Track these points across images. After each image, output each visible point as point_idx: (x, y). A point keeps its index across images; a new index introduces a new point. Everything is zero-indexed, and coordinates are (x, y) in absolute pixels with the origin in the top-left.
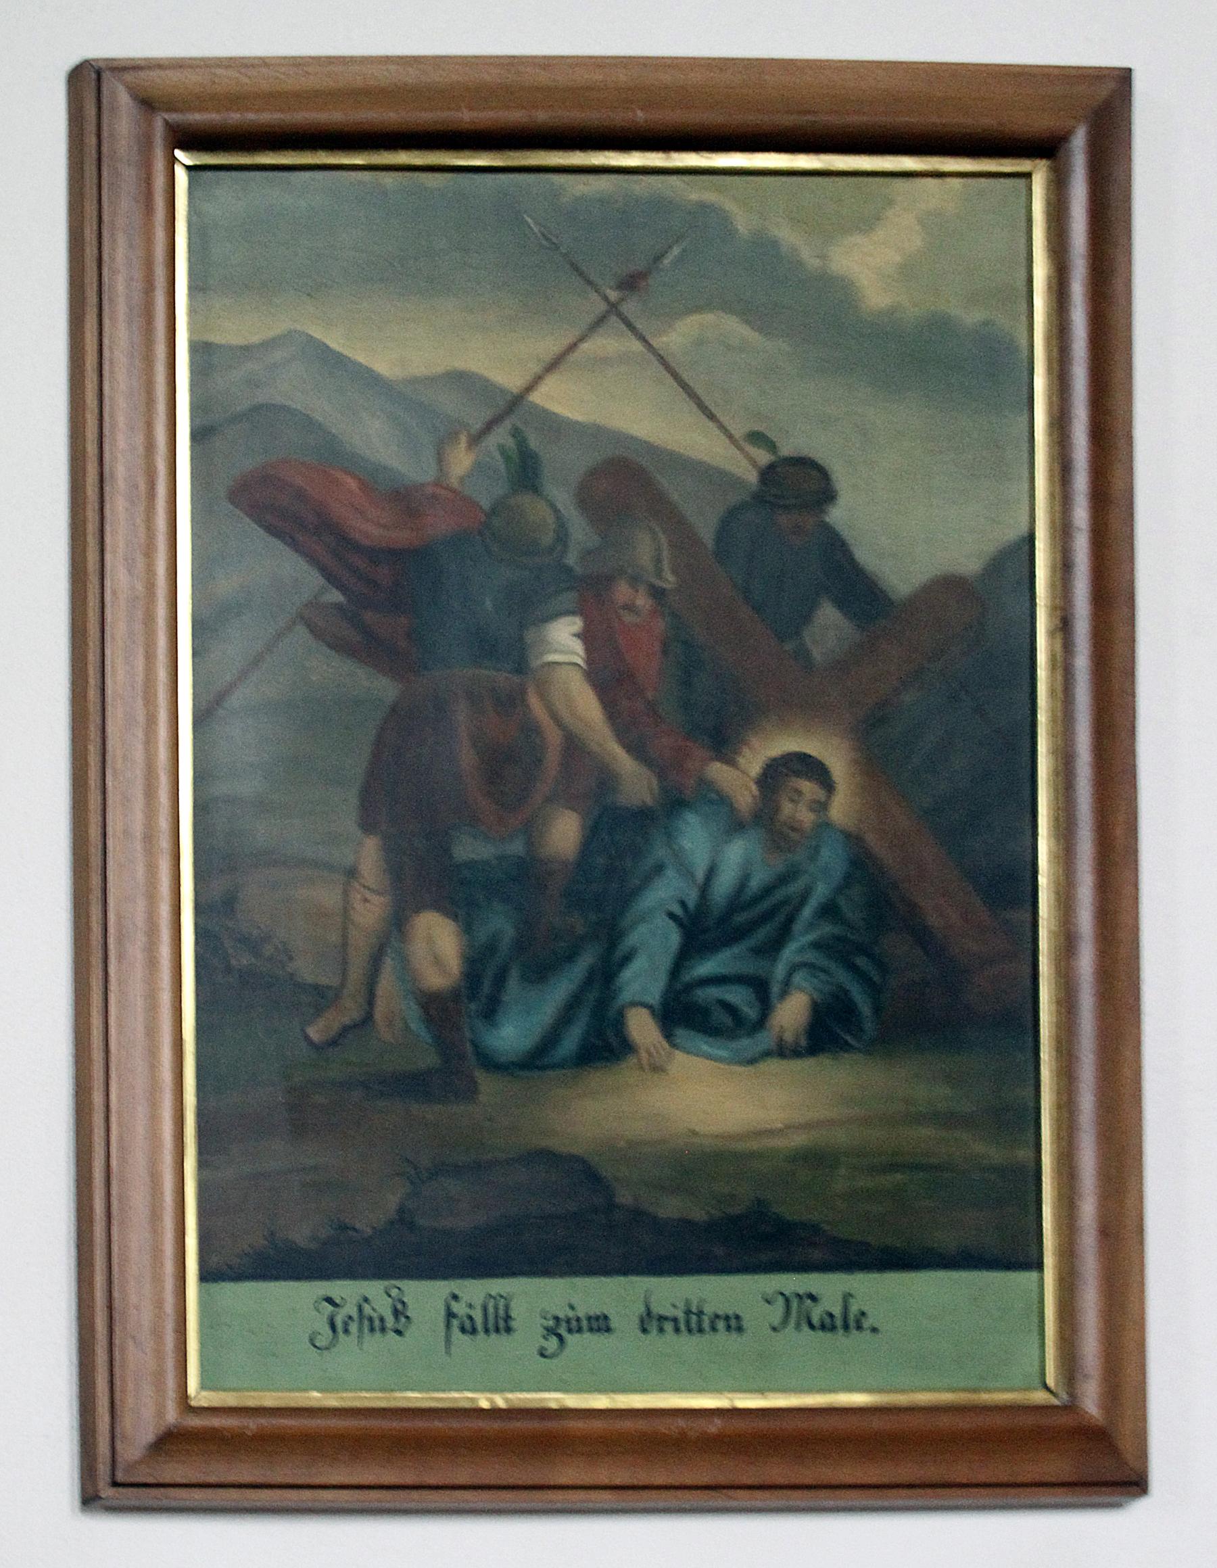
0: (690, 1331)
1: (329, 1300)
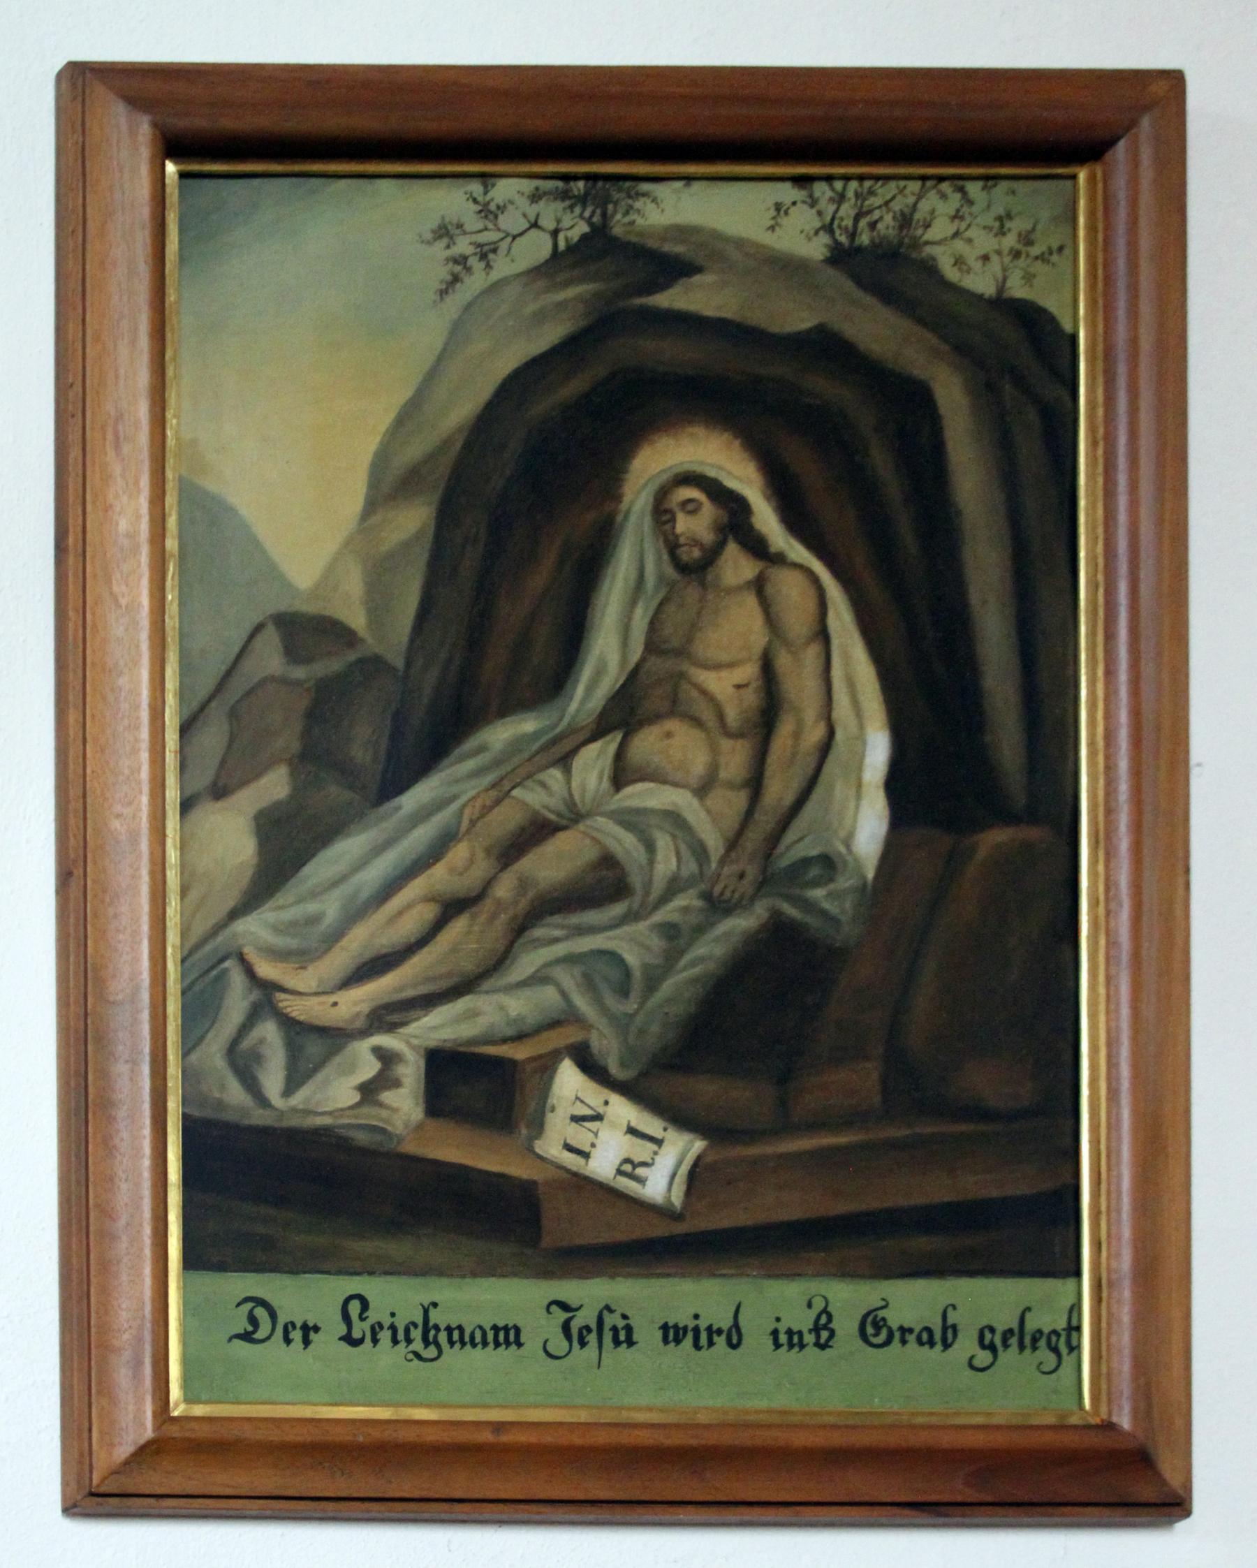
0: (463, 1344)
1: (564, 1306)
